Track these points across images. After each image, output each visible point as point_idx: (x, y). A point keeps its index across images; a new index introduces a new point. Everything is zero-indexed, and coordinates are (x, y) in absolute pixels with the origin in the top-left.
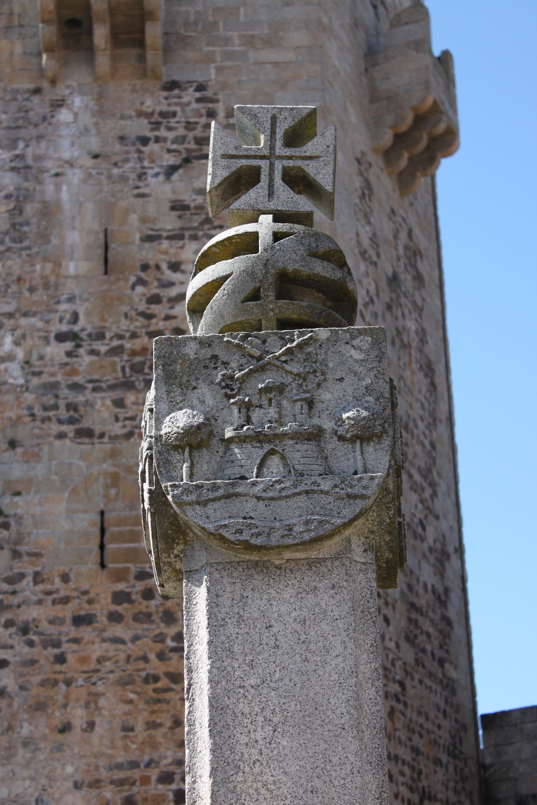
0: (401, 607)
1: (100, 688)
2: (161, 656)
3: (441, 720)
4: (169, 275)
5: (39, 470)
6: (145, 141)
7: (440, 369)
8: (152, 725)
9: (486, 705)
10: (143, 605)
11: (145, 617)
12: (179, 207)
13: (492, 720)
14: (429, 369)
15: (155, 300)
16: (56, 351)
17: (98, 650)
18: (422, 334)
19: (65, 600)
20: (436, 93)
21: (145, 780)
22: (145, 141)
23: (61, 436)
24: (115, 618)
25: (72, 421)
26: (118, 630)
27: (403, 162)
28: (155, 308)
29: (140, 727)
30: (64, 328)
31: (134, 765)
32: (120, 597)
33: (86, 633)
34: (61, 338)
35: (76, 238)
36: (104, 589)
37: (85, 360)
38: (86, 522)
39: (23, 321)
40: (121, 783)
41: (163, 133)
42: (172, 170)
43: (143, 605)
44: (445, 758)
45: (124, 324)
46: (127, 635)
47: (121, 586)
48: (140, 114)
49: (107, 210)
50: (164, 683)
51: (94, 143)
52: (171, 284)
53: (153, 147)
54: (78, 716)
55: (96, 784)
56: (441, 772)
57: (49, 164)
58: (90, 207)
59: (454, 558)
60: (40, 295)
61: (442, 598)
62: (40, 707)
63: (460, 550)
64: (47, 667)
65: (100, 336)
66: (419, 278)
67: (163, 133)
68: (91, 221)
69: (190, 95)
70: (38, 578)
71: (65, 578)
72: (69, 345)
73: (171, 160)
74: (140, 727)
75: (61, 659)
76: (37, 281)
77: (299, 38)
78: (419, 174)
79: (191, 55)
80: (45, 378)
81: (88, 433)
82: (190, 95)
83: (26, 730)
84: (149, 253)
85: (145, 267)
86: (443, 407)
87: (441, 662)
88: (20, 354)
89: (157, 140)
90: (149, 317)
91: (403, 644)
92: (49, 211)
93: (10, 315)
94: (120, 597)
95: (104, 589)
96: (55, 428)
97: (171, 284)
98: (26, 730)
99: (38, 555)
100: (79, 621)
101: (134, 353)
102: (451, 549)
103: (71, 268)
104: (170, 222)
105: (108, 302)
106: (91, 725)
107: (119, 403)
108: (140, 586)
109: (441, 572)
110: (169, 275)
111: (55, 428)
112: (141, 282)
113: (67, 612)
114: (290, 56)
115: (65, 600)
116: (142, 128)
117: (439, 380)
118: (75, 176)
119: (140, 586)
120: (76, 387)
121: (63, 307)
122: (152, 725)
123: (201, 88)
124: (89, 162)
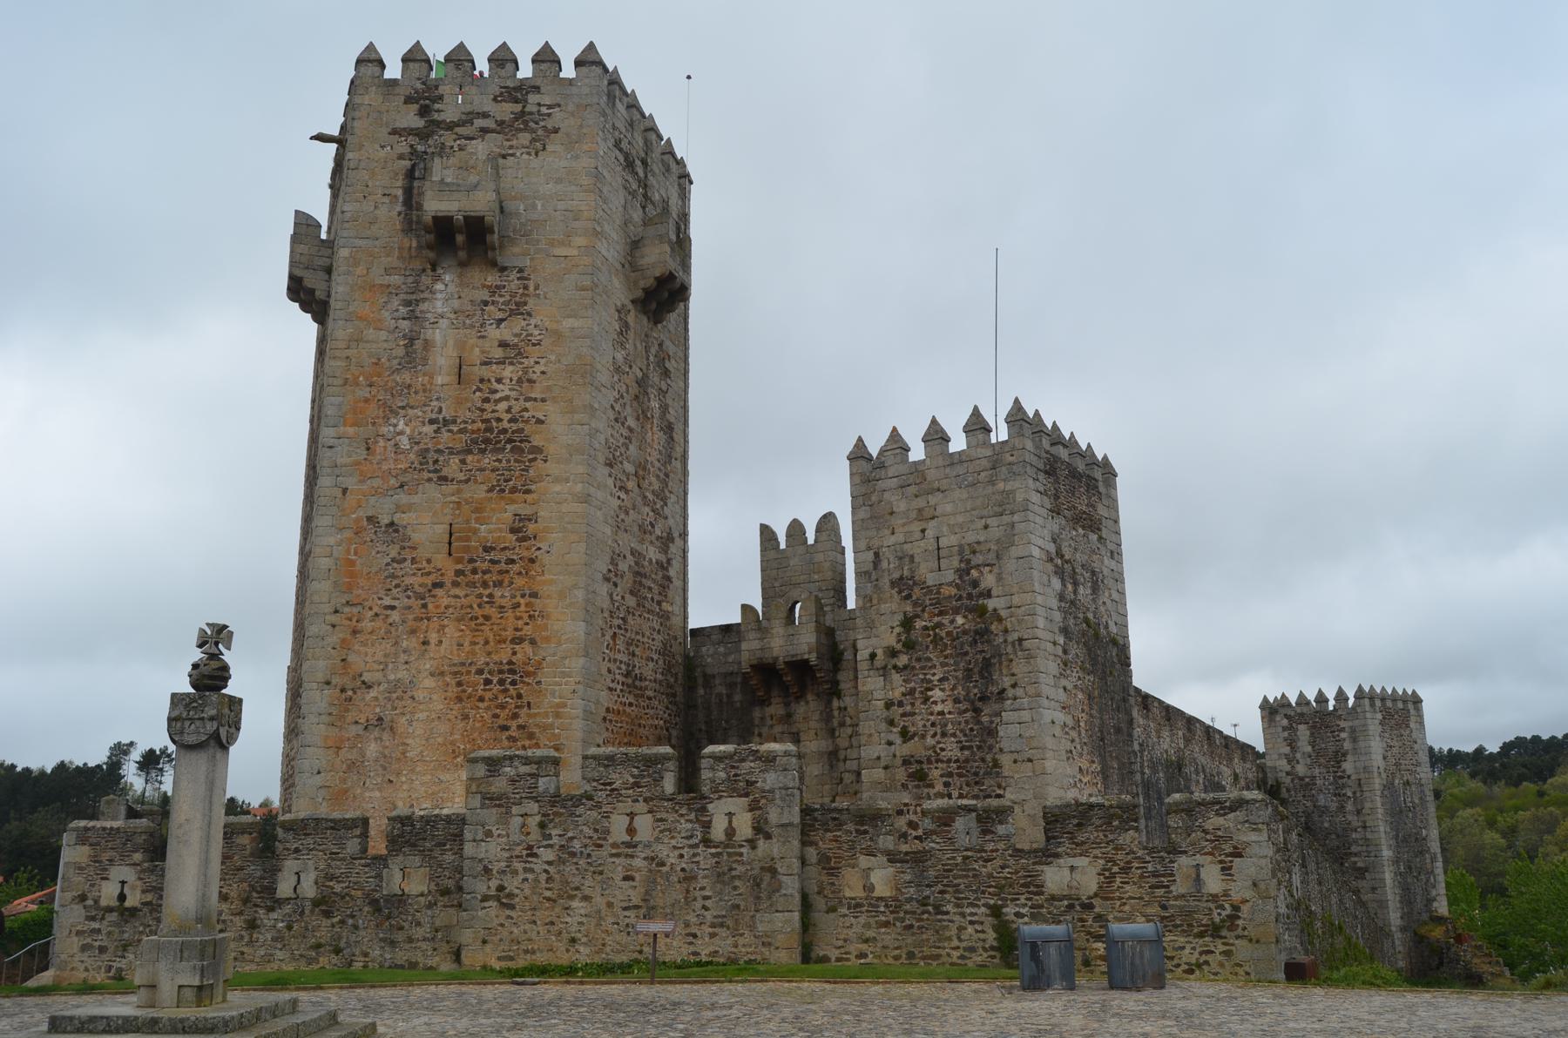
0: (629, 577)
1: (446, 622)
2: (480, 606)
3: (655, 636)
4: (496, 386)
5: (416, 499)
6: (486, 303)
7: (678, 428)
8: (474, 643)
9: (693, 624)
10: (471, 577)
11: (472, 584)
12: (503, 344)
13: (696, 633)
14: (669, 429)
15: (486, 400)
16: (429, 429)
17: (445, 601)
18: (664, 409)
19: (429, 574)
20: (673, 265)
21: (469, 672)
22: (486, 303)
23: (430, 480)
24: (455, 584)
25: (436, 471)
26: (457, 591)
27: (654, 306)
28: (486, 406)
29: (466, 644)
30: (434, 416)
31: (463, 664)
32: (459, 573)
33: (439, 592)
34: (432, 422)
35: (442, 361)
36: (450, 567)
37: (446, 435)
38: (442, 529)
39: (410, 412)
40: (456, 673)
41: (497, 298)
42: (501, 321)
43: (471, 577)
44: (655, 657)
45: (468, 414)
46: (462, 594)
47: (460, 567)
48: (484, 286)
49: (461, 345)
50: (481, 620)
51: (456, 304)
52: (496, 391)
53: (490, 308)
54: (433, 637)
55: (442, 674)
56: (651, 665)
57: (429, 315)
58: (451, 342)
59: (679, 542)
60: (421, 397)
61: (663, 567)
62: (413, 632)
63: (684, 535)
64: (418, 611)
65: (454, 422)
66: (666, 373)
67: (497, 298)
68: (451, 352)
69: (514, 275)
70: (414, 561)
71: (429, 561)
72: (435, 427)
73: (501, 315)
74: (466, 644)
75: (425, 606)
76: (420, 387)
77: (580, 241)
78: (19, 769)
79: (516, 250)
80: (422, 446)
81: (445, 479)
82: (514, 275)
83: (405, 644)
84: (485, 372)
85: (482, 380)
86: (679, 450)
87: (659, 603)
88: (408, 431)
89: (493, 303)
90: (483, 410)
91: (627, 596)
92: (428, 345)
93: (403, 408)
94: (459, 573)
95: (450, 567)
96: (426, 475)
97: (496, 391)
98: (405, 644)
99: (414, 548)
100: (436, 585)
101: (473, 432)
102: (676, 535)
103: (439, 380)
104: (498, 353)
105: (459, 402)
106: (441, 642)
107: (463, 462)
108: (470, 567)
109: (665, 549)
110: (496, 386)
111: (426, 475)
112: (479, 389)
113: (429, 581)
114: (575, 252)
115: (429, 574)
116: (484, 295)
117: (678, 437)
118: (444, 323)
119: (470, 567)
120: (439, 451)
121: (434, 403)
122: (474, 643)
123: (521, 271)
124: (453, 316)
